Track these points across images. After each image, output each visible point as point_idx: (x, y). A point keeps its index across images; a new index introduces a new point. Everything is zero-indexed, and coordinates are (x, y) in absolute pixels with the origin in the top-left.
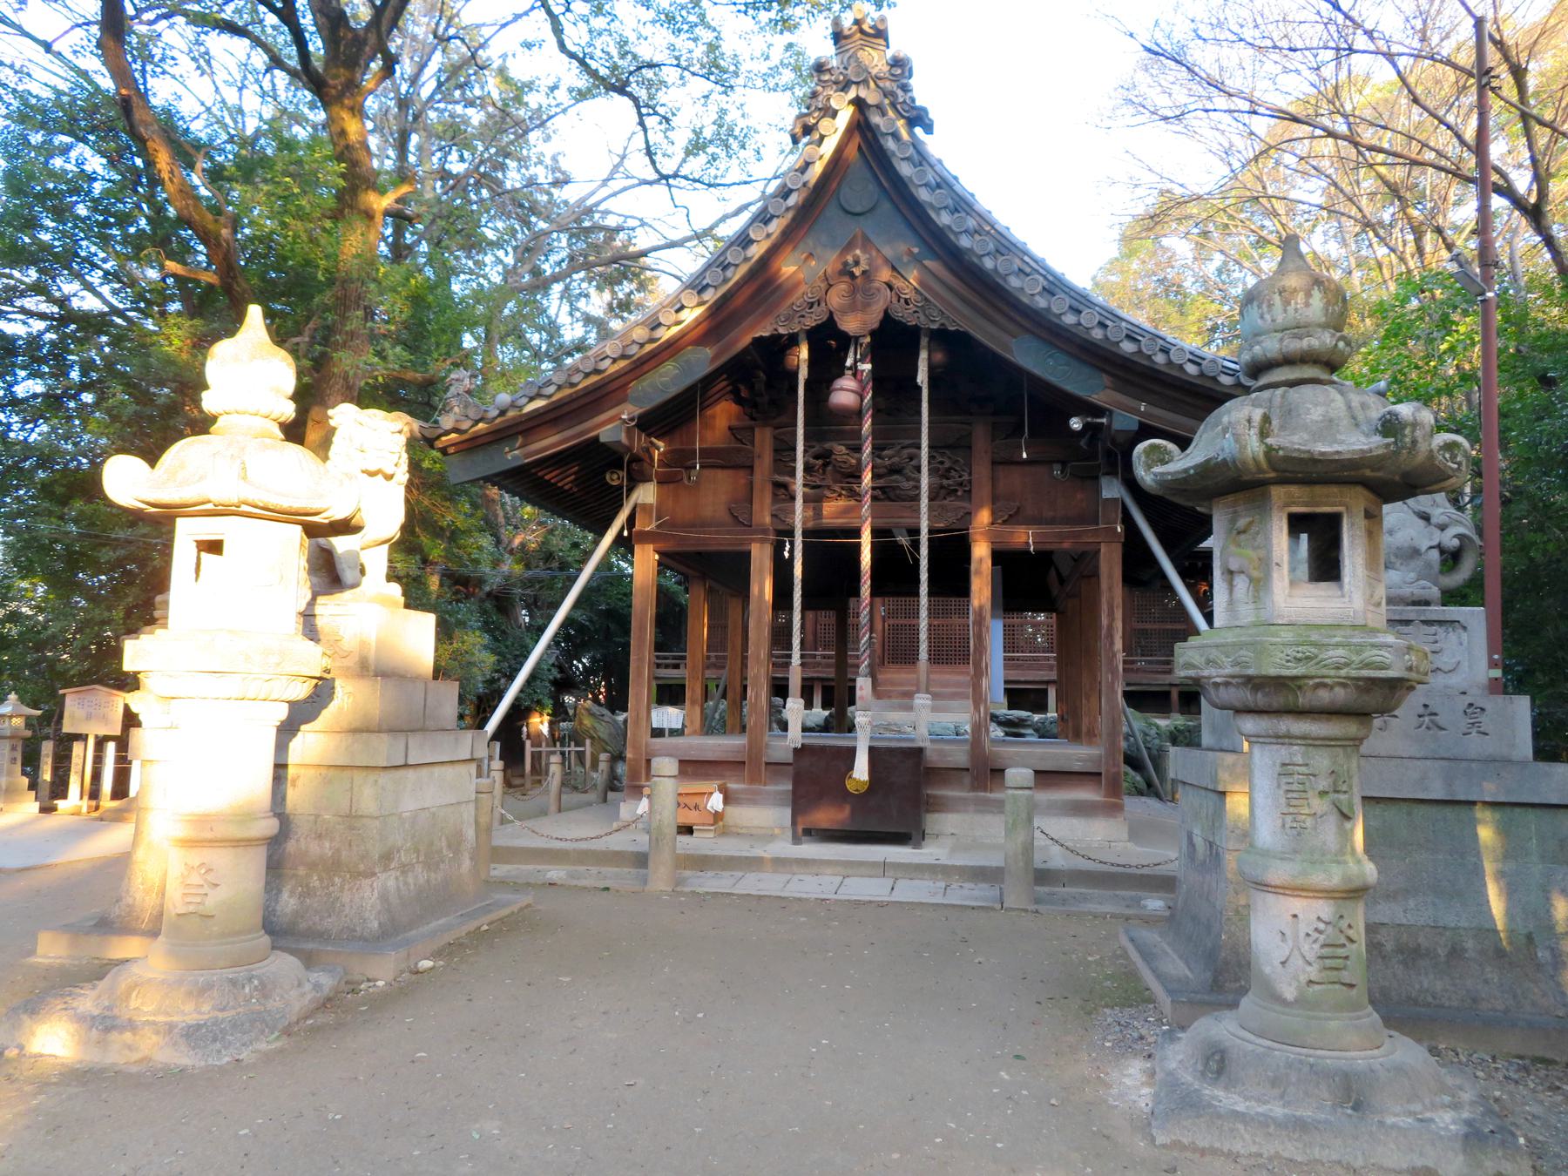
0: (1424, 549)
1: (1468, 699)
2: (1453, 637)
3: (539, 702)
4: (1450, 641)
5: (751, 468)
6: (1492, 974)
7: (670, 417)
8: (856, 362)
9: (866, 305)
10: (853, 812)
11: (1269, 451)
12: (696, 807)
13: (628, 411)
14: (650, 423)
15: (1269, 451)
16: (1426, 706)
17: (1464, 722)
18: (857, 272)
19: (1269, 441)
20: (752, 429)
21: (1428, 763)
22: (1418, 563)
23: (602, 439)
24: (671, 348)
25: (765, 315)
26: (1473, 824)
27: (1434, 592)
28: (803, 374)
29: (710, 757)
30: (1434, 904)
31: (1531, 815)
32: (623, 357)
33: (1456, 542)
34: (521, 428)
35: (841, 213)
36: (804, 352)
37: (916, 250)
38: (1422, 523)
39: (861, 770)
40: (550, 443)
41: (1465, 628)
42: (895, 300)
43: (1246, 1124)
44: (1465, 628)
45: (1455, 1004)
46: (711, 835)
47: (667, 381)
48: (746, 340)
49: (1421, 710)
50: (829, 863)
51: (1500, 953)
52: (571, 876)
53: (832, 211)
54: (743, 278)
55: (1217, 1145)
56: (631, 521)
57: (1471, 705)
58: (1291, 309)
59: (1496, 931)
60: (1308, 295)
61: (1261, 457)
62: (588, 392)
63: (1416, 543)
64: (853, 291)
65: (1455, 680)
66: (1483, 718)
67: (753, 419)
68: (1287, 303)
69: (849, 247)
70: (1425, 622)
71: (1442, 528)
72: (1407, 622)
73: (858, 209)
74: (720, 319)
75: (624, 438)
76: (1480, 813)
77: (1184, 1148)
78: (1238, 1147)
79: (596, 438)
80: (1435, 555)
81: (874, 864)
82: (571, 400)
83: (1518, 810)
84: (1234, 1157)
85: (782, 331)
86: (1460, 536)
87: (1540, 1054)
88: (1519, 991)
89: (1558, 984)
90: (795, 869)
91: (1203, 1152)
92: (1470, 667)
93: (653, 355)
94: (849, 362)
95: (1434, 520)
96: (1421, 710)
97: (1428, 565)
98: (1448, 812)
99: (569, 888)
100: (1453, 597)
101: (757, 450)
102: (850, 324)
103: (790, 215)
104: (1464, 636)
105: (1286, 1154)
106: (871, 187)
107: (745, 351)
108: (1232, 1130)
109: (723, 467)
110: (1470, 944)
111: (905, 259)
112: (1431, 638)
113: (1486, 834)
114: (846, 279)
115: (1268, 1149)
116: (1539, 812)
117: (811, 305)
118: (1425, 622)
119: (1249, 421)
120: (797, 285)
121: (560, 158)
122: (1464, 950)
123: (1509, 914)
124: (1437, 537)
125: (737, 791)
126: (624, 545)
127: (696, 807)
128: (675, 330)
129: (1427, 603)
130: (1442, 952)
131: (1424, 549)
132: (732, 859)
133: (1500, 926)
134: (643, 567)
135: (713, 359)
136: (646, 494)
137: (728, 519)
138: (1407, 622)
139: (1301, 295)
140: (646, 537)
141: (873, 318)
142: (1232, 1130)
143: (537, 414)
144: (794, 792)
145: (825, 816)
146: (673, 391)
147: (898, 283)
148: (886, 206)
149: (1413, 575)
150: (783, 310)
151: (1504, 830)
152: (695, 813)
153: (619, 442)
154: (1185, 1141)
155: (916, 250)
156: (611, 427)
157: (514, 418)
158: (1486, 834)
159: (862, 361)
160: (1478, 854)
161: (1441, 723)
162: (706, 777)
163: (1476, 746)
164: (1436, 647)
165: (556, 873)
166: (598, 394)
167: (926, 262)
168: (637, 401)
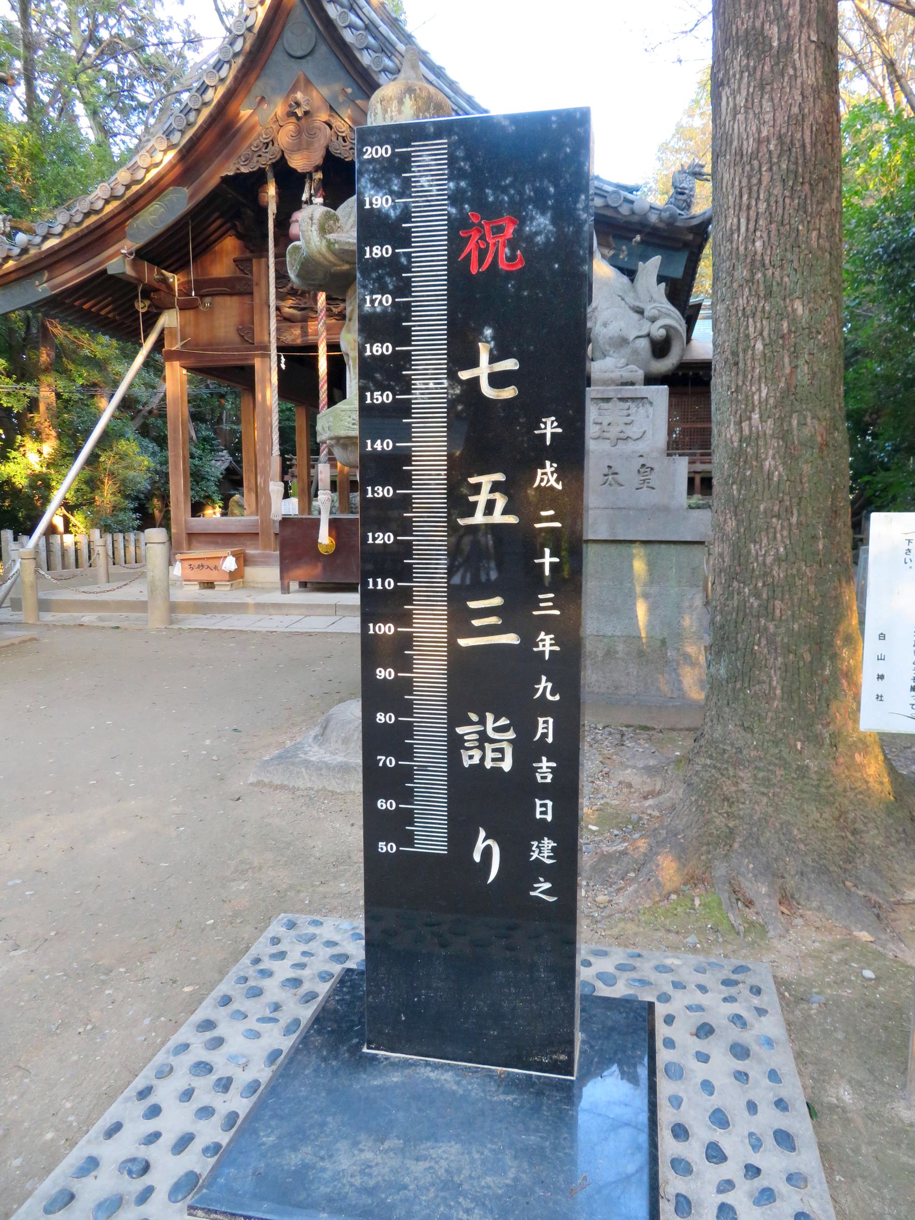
0: (631, 338)
1: (642, 461)
2: (642, 411)
3: (208, 497)
4: (639, 413)
5: (251, 294)
6: (633, 669)
7: (165, 251)
8: (311, 196)
9: (309, 145)
10: (324, 569)
11: (330, 244)
12: (216, 568)
13: (127, 246)
14: (147, 254)
15: (330, 244)
16: (610, 467)
17: (637, 479)
18: (300, 113)
19: (332, 236)
20: (250, 260)
21: (598, 511)
22: (627, 350)
23: (110, 272)
24: (153, 191)
25: (228, 158)
26: (631, 558)
27: (640, 374)
28: (272, 209)
29: (233, 530)
30: (598, 619)
31: (673, 548)
32: (114, 198)
33: (663, 332)
34: (43, 264)
35: (286, 58)
36: (272, 190)
37: (349, 90)
38: (636, 316)
39: (324, 538)
40: (70, 276)
41: (651, 403)
42: (334, 139)
43: (307, 768)
44: (651, 403)
45: (602, 691)
46: (228, 588)
47: (154, 219)
48: (215, 182)
49: (606, 471)
50: (296, 606)
51: (641, 654)
52: (101, 619)
53: (278, 56)
54: (205, 122)
55: (286, 783)
56: (159, 344)
57: (643, 465)
58: (388, 116)
59: (640, 638)
60: (401, 102)
61: (324, 250)
62: (91, 231)
63: (624, 333)
64: (299, 132)
65: (641, 447)
66: (653, 476)
67: (252, 252)
68: (385, 111)
69: (294, 89)
70: (621, 399)
71: (653, 320)
72: (608, 400)
73: (299, 53)
74: (191, 160)
75: (129, 271)
76: (637, 550)
77: (265, 785)
78: (300, 784)
79: (105, 271)
80: (644, 344)
81: (328, 606)
82: (77, 239)
83: (663, 546)
84: (293, 790)
85: (244, 170)
86: (667, 327)
87: (643, 724)
88: (649, 681)
89: (678, 675)
90: (272, 611)
91: (276, 788)
92: (653, 435)
93: (138, 197)
94: (305, 197)
95: (646, 314)
96: (606, 471)
97: (635, 352)
98: (613, 548)
99: (98, 627)
100: (650, 380)
101: (255, 278)
102: (298, 163)
103: (240, 60)
104: (651, 410)
105: (330, 788)
106: (309, 31)
107: (218, 187)
108: (298, 773)
109: (231, 295)
110: (620, 647)
111: (341, 99)
112: (625, 412)
113: (639, 566)
114: (293, 119)
115: (318, 785)
116: (678, 547)
117: (267, 145)
118: (621, 399)
119: (311, 219)
120: (252, 128)
121: (191, 20)
122: (616, 652)
123: (650, 625)
124: (646, 327)
125: (253, 556)
126: (153, 366)
127: (216, 568)
128: (154, 172)
129: (632, 384)
130: (600, 654)
131: (631, 338)
132: (226, 604)
133: (643, 635)
134: (176, 380)
135: (191, 197)
136: (169, 319)
137: (237, 339)
138: (608, 400)
139: (395, 102)
140: (172, 356)
141: (317, 158)
142: (298, 773)
143: (53, 252)
144: (281, 554)
145: (303, 572)
146: (160, 228)
147: (337, 123)
148: (323, 49)
149: (623, 361)
150: (243, 150)
151: (651, 565)
152: (215, 572)
153: (124, 273)
154: (266, 780)
155: (349, 90)
156: (118, 260)
157: (35, 255)
158: (639, 566)
159: (315, 196)
160: (632, 582)
161: (621, 481)
162: (225, 545)
163: (645, 497)
164: (628, 420)
165: (89, 618)
166: (99, 233)
167: (358, 102)
168: (133, 238)
